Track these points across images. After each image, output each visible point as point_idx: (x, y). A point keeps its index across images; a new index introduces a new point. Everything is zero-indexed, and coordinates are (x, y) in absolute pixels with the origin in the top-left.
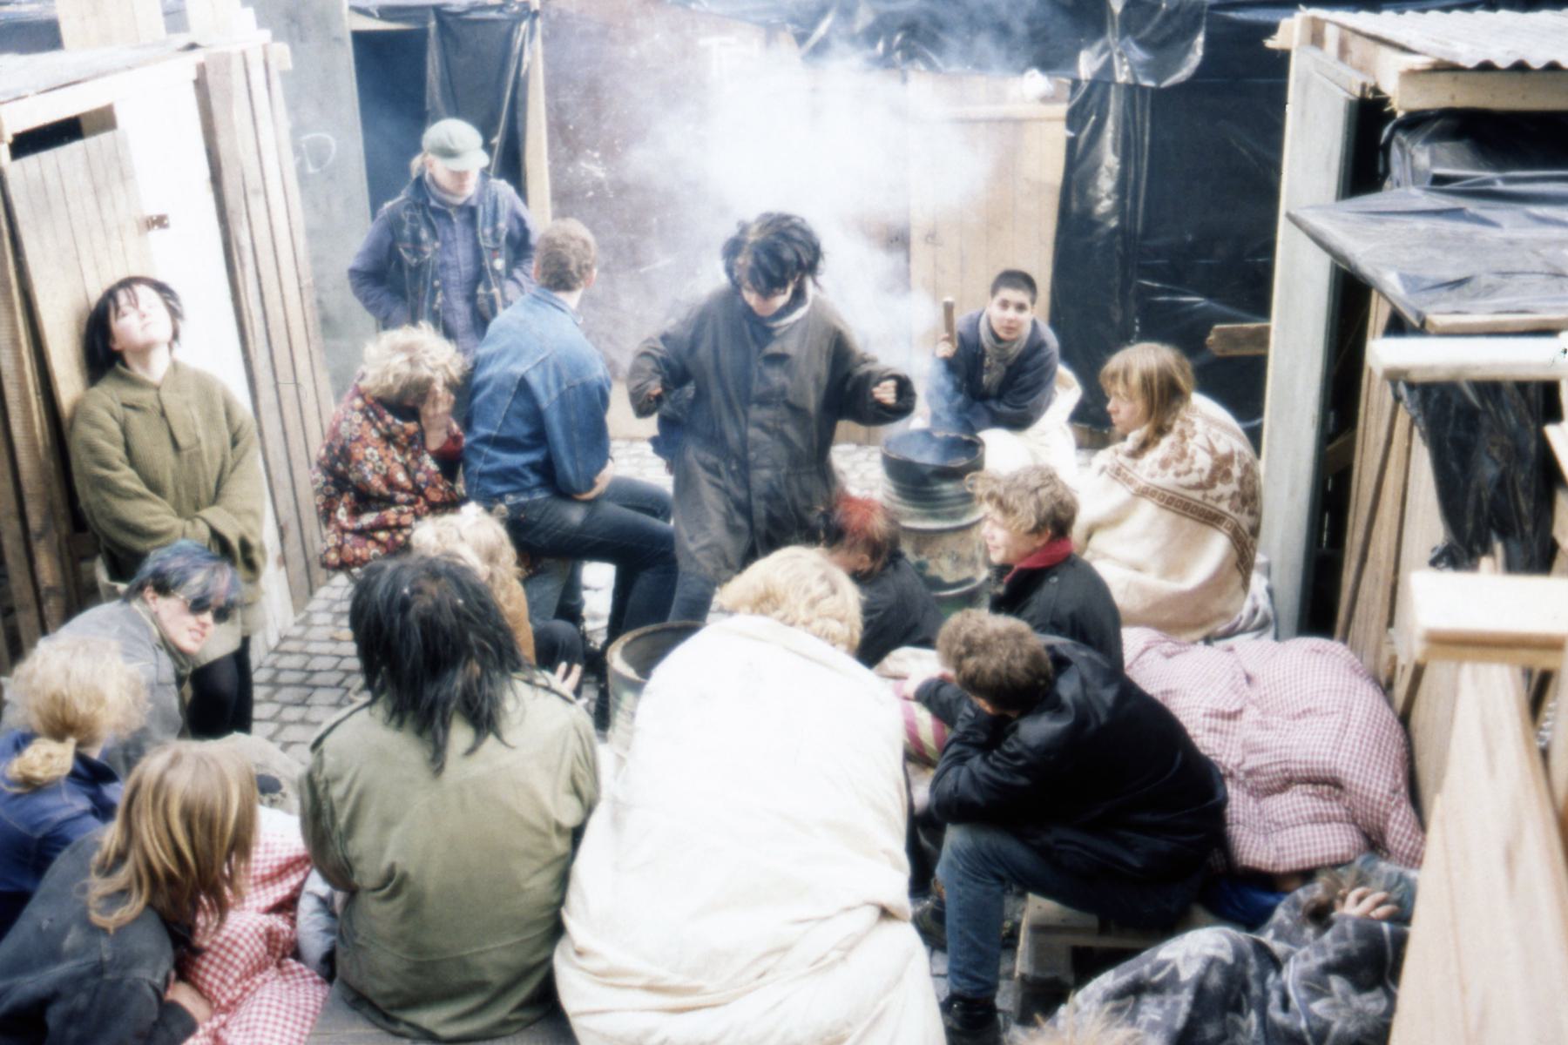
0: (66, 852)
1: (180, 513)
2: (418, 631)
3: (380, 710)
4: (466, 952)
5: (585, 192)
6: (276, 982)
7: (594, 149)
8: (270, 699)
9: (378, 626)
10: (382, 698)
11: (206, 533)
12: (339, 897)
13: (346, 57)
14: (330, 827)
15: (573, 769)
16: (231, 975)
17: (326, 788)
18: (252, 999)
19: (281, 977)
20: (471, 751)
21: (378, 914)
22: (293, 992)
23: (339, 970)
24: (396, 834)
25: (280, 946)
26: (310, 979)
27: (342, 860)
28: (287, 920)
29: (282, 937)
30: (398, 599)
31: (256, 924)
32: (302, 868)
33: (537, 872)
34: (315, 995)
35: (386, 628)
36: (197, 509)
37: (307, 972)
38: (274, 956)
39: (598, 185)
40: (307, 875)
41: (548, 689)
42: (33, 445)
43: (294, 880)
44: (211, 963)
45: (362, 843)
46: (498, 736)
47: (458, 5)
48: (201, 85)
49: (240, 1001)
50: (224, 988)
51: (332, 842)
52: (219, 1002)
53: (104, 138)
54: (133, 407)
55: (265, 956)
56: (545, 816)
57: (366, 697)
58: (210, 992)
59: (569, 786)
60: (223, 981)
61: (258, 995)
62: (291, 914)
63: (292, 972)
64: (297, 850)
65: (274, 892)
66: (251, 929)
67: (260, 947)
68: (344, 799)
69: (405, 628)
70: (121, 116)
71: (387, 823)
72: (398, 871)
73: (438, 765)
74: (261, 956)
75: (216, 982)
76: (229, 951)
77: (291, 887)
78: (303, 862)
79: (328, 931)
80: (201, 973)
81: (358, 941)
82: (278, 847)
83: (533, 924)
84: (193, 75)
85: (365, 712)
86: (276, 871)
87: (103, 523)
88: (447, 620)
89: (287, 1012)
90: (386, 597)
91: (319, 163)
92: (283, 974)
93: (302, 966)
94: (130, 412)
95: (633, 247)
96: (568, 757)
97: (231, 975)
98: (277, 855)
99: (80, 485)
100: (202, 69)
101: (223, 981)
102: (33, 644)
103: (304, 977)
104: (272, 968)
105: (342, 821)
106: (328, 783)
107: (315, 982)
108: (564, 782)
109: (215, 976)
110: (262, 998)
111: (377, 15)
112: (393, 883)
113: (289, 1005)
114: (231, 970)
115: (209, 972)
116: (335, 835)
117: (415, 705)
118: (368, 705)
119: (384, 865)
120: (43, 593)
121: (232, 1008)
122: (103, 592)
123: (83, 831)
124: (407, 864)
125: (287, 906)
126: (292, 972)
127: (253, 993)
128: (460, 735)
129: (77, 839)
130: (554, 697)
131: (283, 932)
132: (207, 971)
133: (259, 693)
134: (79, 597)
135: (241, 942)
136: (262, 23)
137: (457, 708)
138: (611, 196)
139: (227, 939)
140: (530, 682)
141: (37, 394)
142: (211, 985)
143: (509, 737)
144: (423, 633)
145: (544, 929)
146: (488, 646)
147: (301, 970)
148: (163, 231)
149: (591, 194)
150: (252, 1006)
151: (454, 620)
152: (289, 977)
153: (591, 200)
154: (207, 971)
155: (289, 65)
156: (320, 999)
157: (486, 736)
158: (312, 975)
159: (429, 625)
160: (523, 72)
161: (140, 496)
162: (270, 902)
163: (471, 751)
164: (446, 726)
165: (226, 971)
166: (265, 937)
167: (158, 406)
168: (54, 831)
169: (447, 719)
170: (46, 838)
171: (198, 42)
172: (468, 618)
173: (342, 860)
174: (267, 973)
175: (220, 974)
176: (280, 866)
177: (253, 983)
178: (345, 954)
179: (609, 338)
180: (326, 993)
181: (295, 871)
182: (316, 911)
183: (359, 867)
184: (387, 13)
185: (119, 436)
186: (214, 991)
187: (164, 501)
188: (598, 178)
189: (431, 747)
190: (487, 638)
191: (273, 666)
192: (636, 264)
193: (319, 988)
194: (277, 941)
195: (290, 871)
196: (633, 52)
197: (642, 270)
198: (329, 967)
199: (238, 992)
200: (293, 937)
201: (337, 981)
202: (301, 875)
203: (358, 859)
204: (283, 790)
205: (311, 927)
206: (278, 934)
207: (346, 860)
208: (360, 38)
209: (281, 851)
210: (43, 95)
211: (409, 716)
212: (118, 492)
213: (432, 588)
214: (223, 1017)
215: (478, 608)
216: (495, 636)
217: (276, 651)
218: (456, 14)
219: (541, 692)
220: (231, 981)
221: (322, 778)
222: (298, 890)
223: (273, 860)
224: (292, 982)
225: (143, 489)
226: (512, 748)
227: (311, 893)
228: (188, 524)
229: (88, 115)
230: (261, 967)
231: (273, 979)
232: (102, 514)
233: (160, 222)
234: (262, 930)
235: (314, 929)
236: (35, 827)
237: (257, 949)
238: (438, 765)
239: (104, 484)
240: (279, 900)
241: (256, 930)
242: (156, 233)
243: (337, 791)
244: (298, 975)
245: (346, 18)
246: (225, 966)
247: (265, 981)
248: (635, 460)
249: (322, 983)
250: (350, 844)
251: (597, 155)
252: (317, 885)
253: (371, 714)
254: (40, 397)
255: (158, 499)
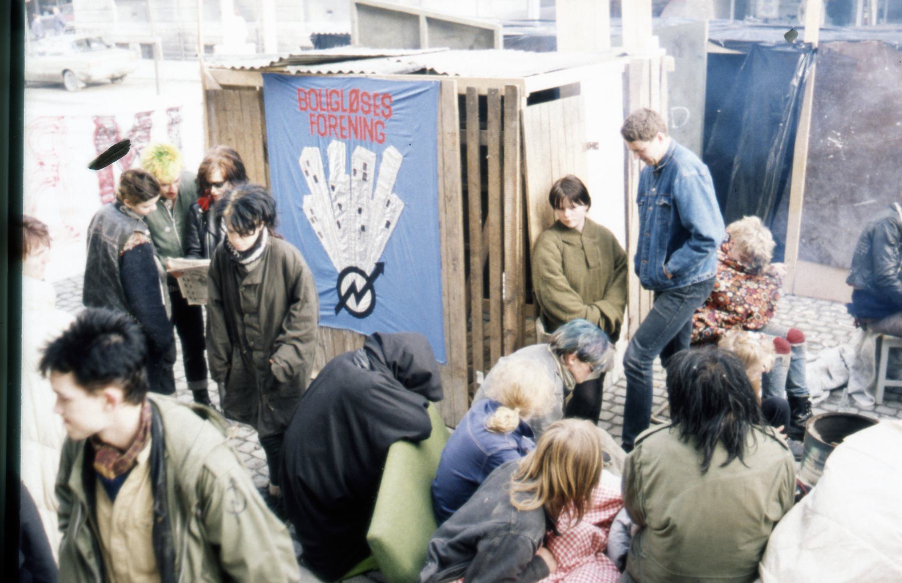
0: (498, 468)
1: (585, 301)
2: (700, 391)
3: (676, 431)
4: (700, 576)
5: (828, 155)
6: (594, 564)
7: (838, 131)
8: (609, 410)
9: (680, 385)
10: (679, 425)
11: (598, 314)
12: (634, 527)
13: (703, 64)
14: (638, 489)
15: (781, 486)
16: (570, 552)
17: (640, 468)
18: (579, 569)
19: (596, 562)
20: (724, 465)
21: (654, 543)
22: (601, 571)
23: (627, 567)
24: (674, 502)
25: (599, 544)
26: (611, 567)
27: (642, 509)
28: (604, 532)
29: (600, 540)
30: (691, 372)
31: (588, 529)
32: (617, 506)
33: (749, 542)
34: (613, 577)
35: (683, 386)
36: (594, 301)
37: (610, 563)
38: (594, 549)
39: (837, 152)
40: (619, 511)
41: (773, 437)
42: (514, 255)
43: (612, 512)
44: (562, 543)
45: (654, 502)
46: (741, 459)
47: (770, 43)
48: (626, 76)
49: (573, 568)
50: (566, 559)
51: (638, 498)
52: (562, 565)
53: (573, 99)
54: (568, 243)
55: (589, 548)
56: (759, 508)
57: (669, 422)
58: (558, 558)
59: (777, 497)
60: (566, 554)
61: (583, 568)
62: (607, 529)
63: (602, 561)
64: (616, 495)
65: (600, 515)
66: (585, 531)
67: (588, 542)
68: (649, 475)
69: (694, 389)
70: (583, 89)
71: (670, 495)
72: (671, 523)
73: (705, 468)
74: (587, 547)
75: (562, 554)
76: (572, 539)
77: (609, 515)
78: (618, 503)
79: (625, 544)
80: (555, 547)
81: (642, 554)
82: (606, 492)
83: (741, 570)
84: (623, 70)
85: (667, 430)
86: (603, 504)
87: (545, 302)
88: (718, 386)
89: (592, 578)
90: (685, 369)
91: (679, 123)
92: (597, 560)
93: (608, 559)
94: (567, 246)
95: (853, 191)
96: (779, 481)
97: (570, 552)
98: (605, 496)
99: (535, 278)
100: (627, 67)
101: (566, 554)
102: (496, 361)
103: (608, 565)
104: (592, 555)
105: (646, 487)
106: (641, 465)
107: (613, 569)
108: (774, 494)
109: (562, 550)
110: (585, 570)
111: (723, 45)
112: (667, 528)
113: (598, 578)
114: (571, 550)
115: (559, 546)
116: (640, 494)
117: (695, 432)
118: (670, 427)
119: (664, 518)
120: (505, 331)
121: (568, 570)
122: (539, 338)
123: (511, 458)
124: (678, 521)
125: (605, 525)
126: (602, 561)
127: (581, 566)
128: (719, 454)
129: (508, 461)
130: (776, 444)
131: (601, 538)
132: (558, 547)
133: (604, 405)
134: (522, 340)
135: (579, 536)
136: (662, 44)
137: (720, 437)
138: (844, 159)
139: (572, 533)
140: (761, 431)
141: (520, 229)
142: (559, 554)
143: (746, 460)
144: (704, 393)
145: (745, 574)
146: (740, 404)
147: (607, 561)
148: (595, 151)
149: (832, 156)
150: (579, 573)
151: (721, 387)
152: (600, 563)
153: (832, 160)
154: (558, 547)
155: (672, 68)
156: (615, 579)
157: (734, 457)
158: (612, 565)
159: (708, 388)
160: (804, 80)
161: (567, 291)
162: (597, 520)
163: (724, 465)
164: (713, 448)
165: (568, 550)
166: (591, 538)
167: (581, 244)
168: (497, 454)
169: (714, 443)
170: (492, 457)
171: (627, 53)
172: (730, 387)
173: (642, 509)
174: (590, 557)
175: (565, 550)
176: (605, 502)
177: (582, 560)
178: (634, 559)
179: (830, 242)
180: (618, 576)
181: (613, 507)
182: (621, 532)
183: (650, 515)
184: (729, 44)
185: (560, 257)
186: (560, 558)
187: (578, 295)
188: (838, 148)
189: (702, 458)
190: (740, 400)
191: (613, 393)
192: (852, 201)
193: (615, 573)
194: (597, 541)
195: (610, 506)
196: (870, 76)
197: (856, 205)
198: (622, 563)
199: (573, 563)
200: (606, 542)
201: (625, 572)
202: (616, 509)
203: (650, 510)
204: (611, 461)
205: (616, 539)
206: (598, 538)
207: (644, 510)
208: (712, 57)
209: (607, 494)
210: (546, 74)
211: (691, 438)
212: (556, 287)
213: (712, 367)
214: (563, 574)
215: (737, 382)
216: (745, 400)
217: (615, 385)
218: (768, 48)
219: (768, 438)
220: (570, 556)
221: (639, 461)
222: (613, 517)
223: (602, 498)
224: (601, 566)
225: (568, 287)
226: (747, 467)
227: (619, 521)
228: (589, 308)
229: (565, 87)
230: (587, 553)
231: (592, 562)
232: (546, 297)
233: (594, 146)
234: (591, 534)
235: (618, 541)
236: (488, 450)
237: (586, 543)
238: (705, 468)
239: (547, 281)
240: (601, 521)
241: (588, 532)
242: (592, 151)
243: (646, 470)
244: (605, 563)
245: (706, 45)
246: (568, 546)
247: (588, 562)
248: (833, 314)
249: (617, 571)
250: (647, 501)
251: (839, 134)
252: (623, 517)
253: (670, 432)
254: (521, 230)
255: (575, 293)
